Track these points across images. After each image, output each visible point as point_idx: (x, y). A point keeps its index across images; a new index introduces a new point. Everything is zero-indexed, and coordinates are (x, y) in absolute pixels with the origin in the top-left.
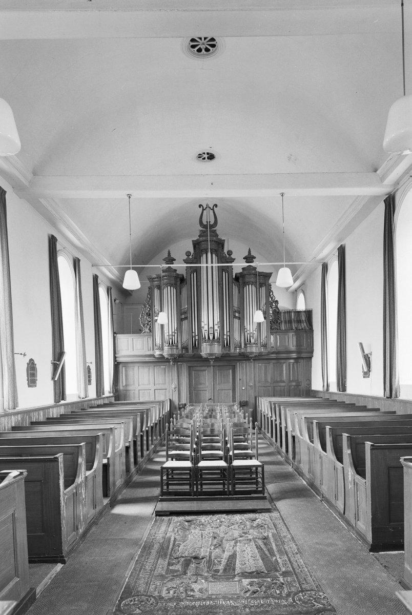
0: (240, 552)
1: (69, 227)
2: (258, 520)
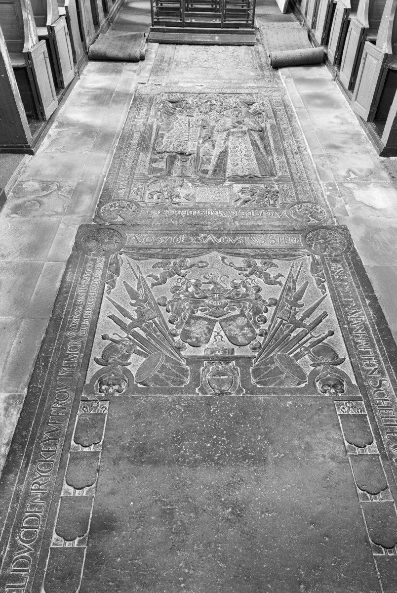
2: (255, 105)
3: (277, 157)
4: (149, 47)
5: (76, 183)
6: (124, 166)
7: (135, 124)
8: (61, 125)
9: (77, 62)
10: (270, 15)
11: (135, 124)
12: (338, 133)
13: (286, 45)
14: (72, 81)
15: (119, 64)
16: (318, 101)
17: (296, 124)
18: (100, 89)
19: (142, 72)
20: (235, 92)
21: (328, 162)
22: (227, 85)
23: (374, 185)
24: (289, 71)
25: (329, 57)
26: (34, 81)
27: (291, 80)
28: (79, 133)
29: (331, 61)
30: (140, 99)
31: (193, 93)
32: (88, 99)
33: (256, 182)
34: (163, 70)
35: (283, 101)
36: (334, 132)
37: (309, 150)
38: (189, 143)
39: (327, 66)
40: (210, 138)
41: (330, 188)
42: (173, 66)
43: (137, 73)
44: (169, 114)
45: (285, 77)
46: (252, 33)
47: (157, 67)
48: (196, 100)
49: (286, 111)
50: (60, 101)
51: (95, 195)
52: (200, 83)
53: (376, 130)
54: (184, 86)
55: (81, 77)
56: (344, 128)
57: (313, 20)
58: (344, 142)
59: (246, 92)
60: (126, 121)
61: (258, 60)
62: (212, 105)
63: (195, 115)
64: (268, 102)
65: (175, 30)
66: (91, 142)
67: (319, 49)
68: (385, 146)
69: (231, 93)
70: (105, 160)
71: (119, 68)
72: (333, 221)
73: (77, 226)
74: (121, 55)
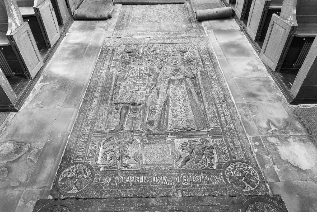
0: (172, 98)
1: (308, 44)
2: (188, 53)
3: (208, 107)
5: (44, 144)
6: (86, 121)
8: (45, 79)
9: (64, 22)
12: (253, 81)
14: (59, 40)
16: (233, 50)
17: (219, 71)
18: (78, 44)
19: (109, 28)
20: (173, 42)
21: (250, 112)
22: (167, 37)
23: (293, 138)
24: (210, 24)
25: (236, 13)
26: (19, 55)
27: (211, 31)
28: (57, 86)
29: (238, 17)
30: (106, 51)
31: (143, 44)
32: (69, 54)
33: (193, 136)
34: (124, 25)
35: (208, 49)
36: (249, 79)
37: (232, 98)
38: (139, 92)
39: (235, 19)
40: (155, 86)
41: (257, 143)
42: (131, 21)
43: (105, 29)
44: (126, 63)
45: (207, 28)
47: (119, 23)
48: (146, 49)
49: (211, 58)
50: (45, 62)
51: (58, 159)
52: (148, 35)
53: (283, 80)
54: (137, 38)
55: (67, 34)
56: (256, 75)
58: (259, 90)
60: (94, 72)
61: (188, 15)
62: (157, 54)
63: (144, 63)
64: (197, 50)
66: (64, 95)
68: (295, 98)
69: (170, 43)
70: (72, 115)
72: (266, 187)
73: (34, 202)
74: (95, 16)
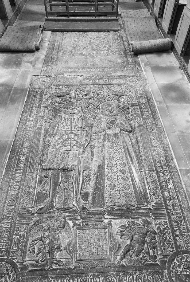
2: (124, 97)
4: (44, 36)
7: (26, 129)
10: (127, 2)
11: (26, 129)
13: (141, 31)
15: (20, 55)
27: (148, 68)
29: (178, 52)
39: (174, 53)
42: (61, 54)
43: (33, 64)
46: (117, 20)
57: (159, 12)
59: (116, 83)
61: (123, 46)
65: (63, 19)
67: (167, 40)
71: (19, 60)
74: (21, 48)
